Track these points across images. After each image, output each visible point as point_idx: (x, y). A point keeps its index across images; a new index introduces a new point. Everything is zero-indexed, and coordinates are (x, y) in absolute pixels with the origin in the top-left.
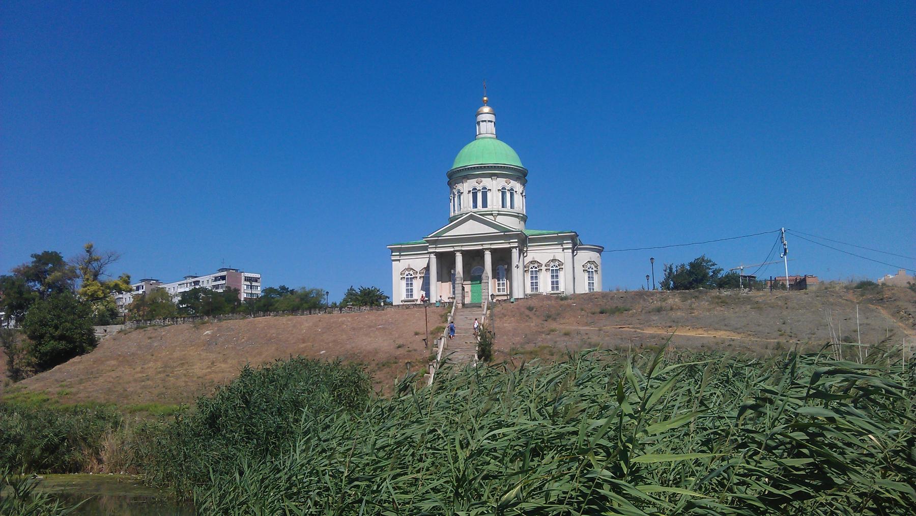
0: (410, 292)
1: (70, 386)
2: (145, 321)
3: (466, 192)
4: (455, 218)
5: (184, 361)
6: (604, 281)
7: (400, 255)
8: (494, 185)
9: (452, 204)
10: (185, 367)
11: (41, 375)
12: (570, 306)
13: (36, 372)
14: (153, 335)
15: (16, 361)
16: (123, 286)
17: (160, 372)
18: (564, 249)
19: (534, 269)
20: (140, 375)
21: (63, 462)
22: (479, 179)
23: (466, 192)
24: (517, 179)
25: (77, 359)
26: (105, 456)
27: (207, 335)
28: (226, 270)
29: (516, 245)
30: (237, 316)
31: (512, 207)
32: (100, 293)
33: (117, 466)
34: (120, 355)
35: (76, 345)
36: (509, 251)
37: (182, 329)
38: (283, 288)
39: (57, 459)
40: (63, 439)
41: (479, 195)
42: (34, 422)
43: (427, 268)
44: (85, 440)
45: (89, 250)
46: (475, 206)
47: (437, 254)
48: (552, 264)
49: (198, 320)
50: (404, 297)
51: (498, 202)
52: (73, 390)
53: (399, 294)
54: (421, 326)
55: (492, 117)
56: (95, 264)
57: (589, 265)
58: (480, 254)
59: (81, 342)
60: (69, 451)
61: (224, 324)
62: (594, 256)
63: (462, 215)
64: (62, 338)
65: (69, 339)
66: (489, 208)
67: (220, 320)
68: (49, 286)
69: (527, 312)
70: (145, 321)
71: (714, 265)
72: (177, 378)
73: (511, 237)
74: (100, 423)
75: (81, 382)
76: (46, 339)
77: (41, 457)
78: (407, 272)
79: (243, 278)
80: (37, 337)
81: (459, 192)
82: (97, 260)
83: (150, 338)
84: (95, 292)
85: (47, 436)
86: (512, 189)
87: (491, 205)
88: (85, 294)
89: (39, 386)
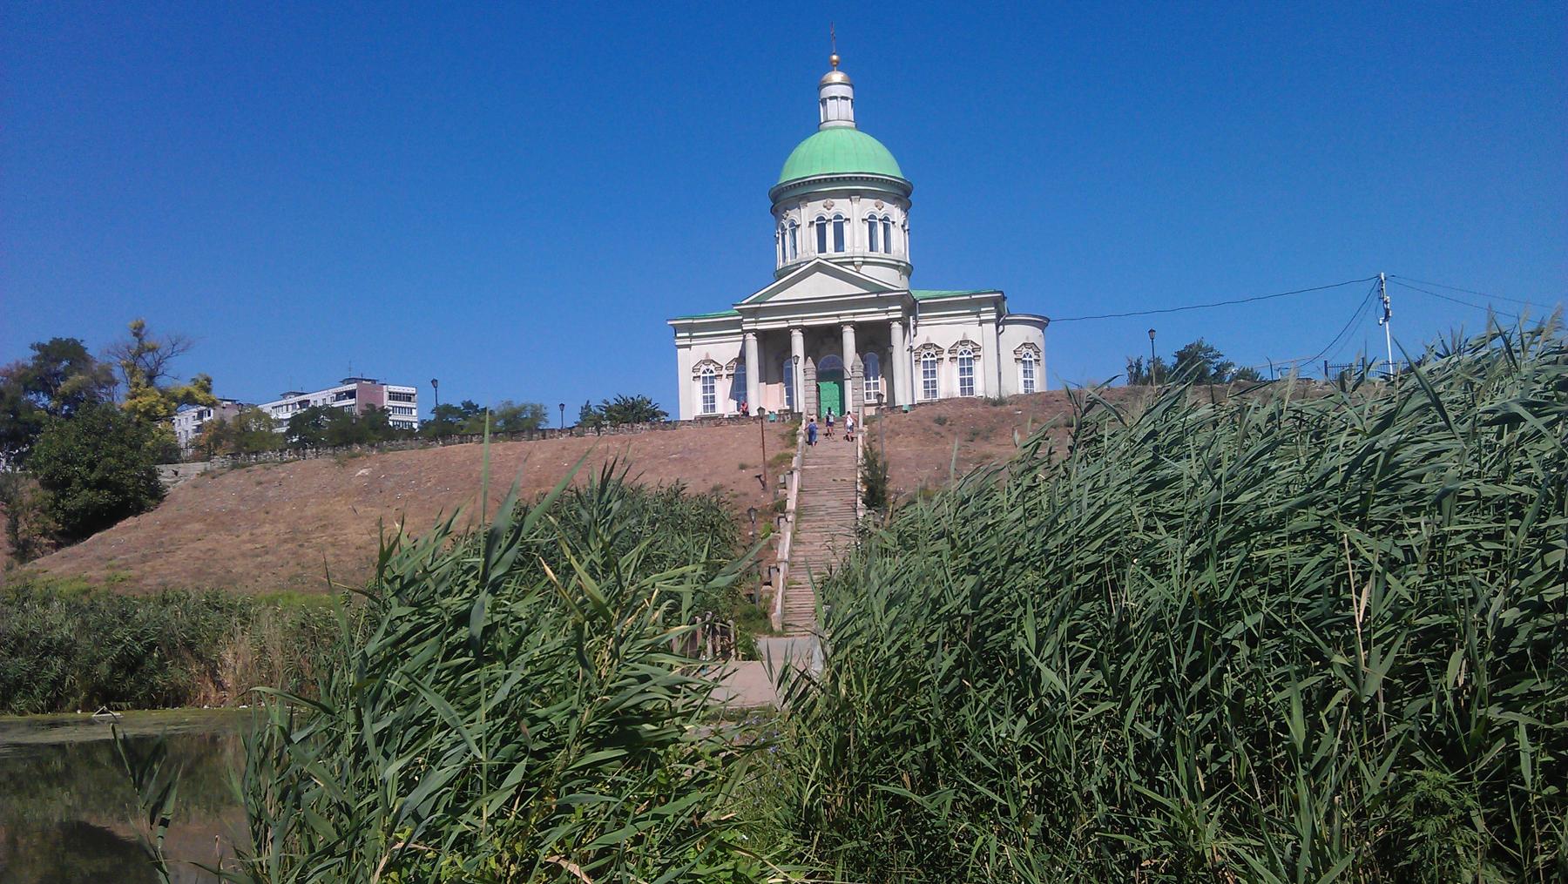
0: (710, 401)
2: (248, 454)
4: (786, 271)
6: (1051, 374)
7: (691, 337)
8: (856, 211)
9: (779, 247)
10: (331, 531)
11: (67, 550)
12: (1010, 415)
13: (58, 546)
14: (263, 479)
15: (23, 526)
16: (200, 396)
17: (285, 541)
18: (981, 323)
19: (929, 357)
20: (249, 546)
21: (152, 688)
22: (829, 201)
24: (895, 200)
25: (130, 521)
26: (229, 681)
27: (363, 476)
28: (355, 380)
30: (414, 444)
32: (160, 408)
34: (209, 514)
35: (127, 496)
36: (885, 327)
37: (318, 466)
38: (469, 405)
39: (140, 682)
40: (151, 647)
41: (830, 229)
42: (91, 617)
43: (741, 359)
44: (190, 646)
45: (138, 332)
46: (822, 248)
47: (758, 333)
48: (961, 349)
50: (699, 411)
51: (862, 241)
52: (133, 573)
53: (691, 403)
54: (753, 455)
55: (847, 91)
56: (149, 358)
57: (1025, 350)
58: (834, 332)
59: (136, 492)
60: (162, 667)
61: (391, 457)
62: (1032, 334)
64: (101, 484)
65: (117, 488)
66: (848, 250)
67: (381, 450)
68: (65, 399)
69: (936, 427)
70: (248, 454)
71: (1218, 356)
72: (321, 549)
74: (215, 616)
75: (144, 559)
76: (74, 486)
77: (110, 679)
78: (704, 368)
79: (386, 395)
80: (57, 484)
81: (792, 224)
82: (153, 349)
83: (260, 483)
85: (120, 642)
86: (886, 219)
87: (847, 247)
89: (65, 568)
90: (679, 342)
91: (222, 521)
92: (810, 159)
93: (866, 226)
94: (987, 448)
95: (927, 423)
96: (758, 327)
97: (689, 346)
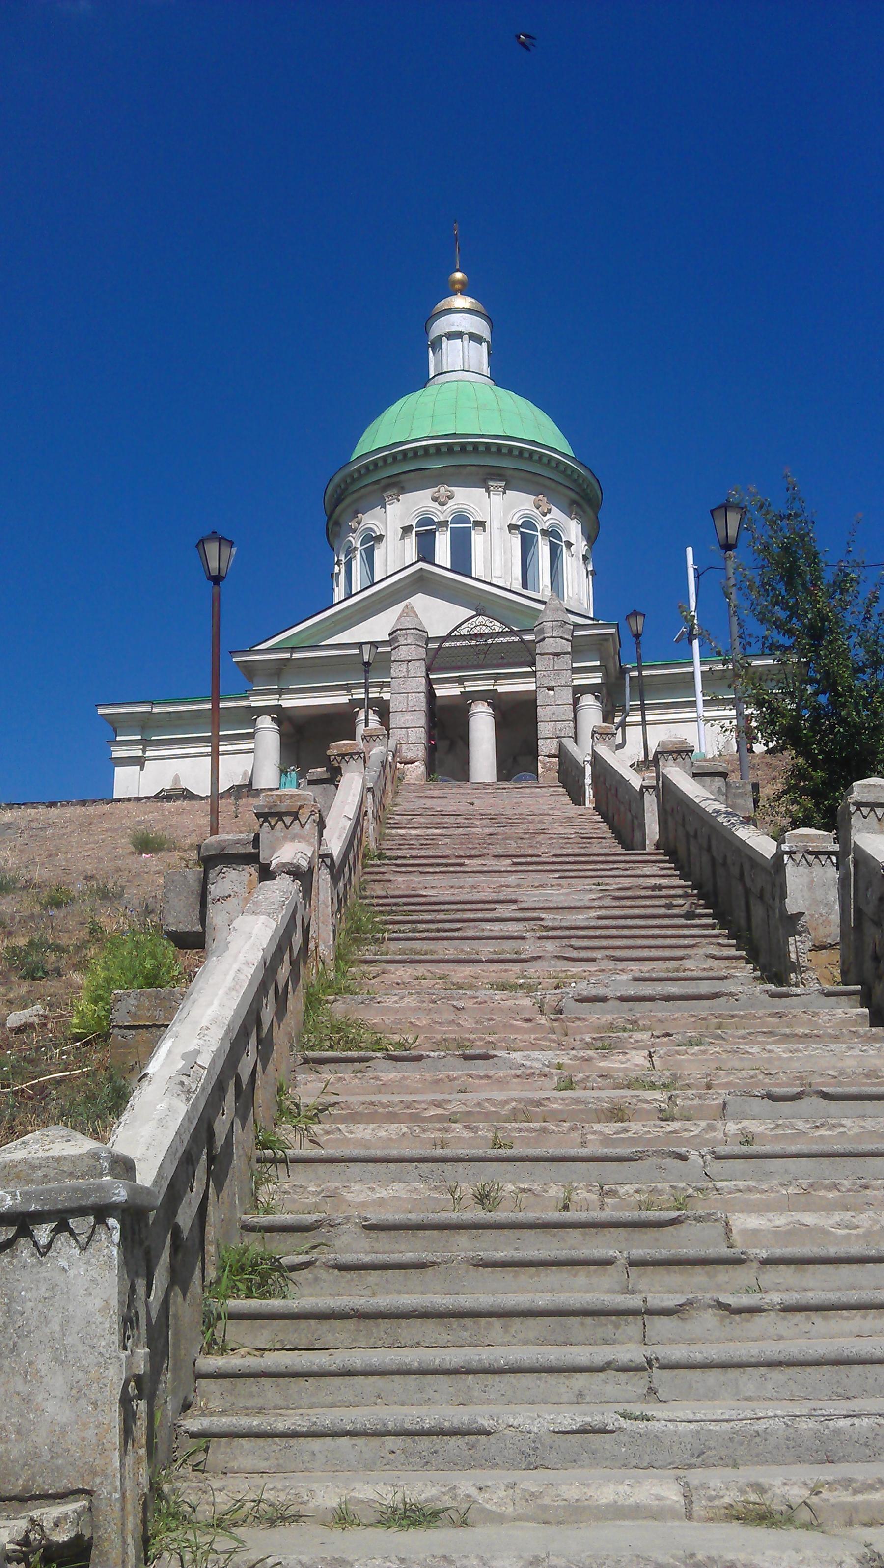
8: (497, 510)
24: (572, 508)
29: (596, 679)
36: (630, 677)
55: (480, 326)
90: (118, 753)
93: (516, 541)
97: (139, 761)
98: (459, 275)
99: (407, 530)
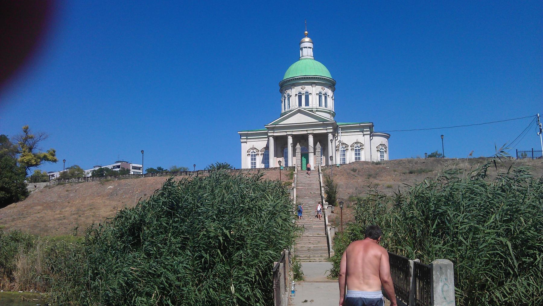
1: (5, 222)
3: (293, 95)
5: (92, 207)
7: (247, 139)
8: (314, 90)
9: (283, 104)
12: (384, 168)
14: (69, 189)
16: (50, 157)
18: (364, 135)
20: (59, 216)
22: (303, 86)
23: (293, 95)
25: (13, 205)
28: (120, 162)
29: (331, 131)
31: (326, 106)
32: (33, 161)
33: (26, 285)
36: (326, 135)
43: (267, 148)
45: (26, 131)
46: (300, 104)
48: (356, 145)
49: (103, 179)
55: (311, 45)
57: (381, 147)
59: (16, 192)
61: (122, 181)
62: (384, 140)
63: (291, 111)
65: (7, 190)
69: (352, 173)
70: (65, 179)
72: (87, 218)
73: (328, 125)
75: (13, 220)
78: (252, 151)
82: (32, 138)
83: (67, 191)
84: (30, 160)
86: (326, 94)
87: (309, 102)
88: (22, 162)
90: (242, 141)
91: (49, 206)
92: (295, 70)
93: (318, 97)
94: (376, 181)
95: (349, 171)
96: (275, 134)
97: (246, 142)
98: (306, 32)
99: (296, 95)
